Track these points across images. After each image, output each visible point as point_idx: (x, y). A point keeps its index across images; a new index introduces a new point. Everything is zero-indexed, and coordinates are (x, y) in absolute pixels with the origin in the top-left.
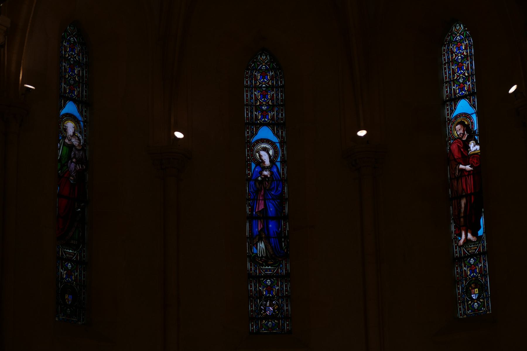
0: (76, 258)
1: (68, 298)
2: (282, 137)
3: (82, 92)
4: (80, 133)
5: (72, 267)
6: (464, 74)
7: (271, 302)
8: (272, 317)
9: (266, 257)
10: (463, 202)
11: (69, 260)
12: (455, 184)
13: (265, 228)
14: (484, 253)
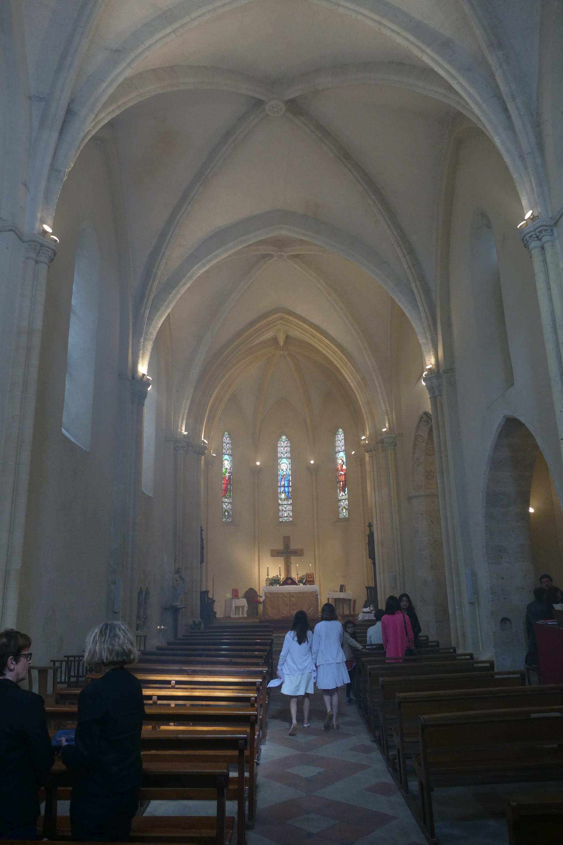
1: (226, 514)
7: (286, 512)
8: (287, 517)
9: (285, 499)
10: (341, 483)
11: (226, 502)
13: (285, 490)
14: (347, 499)
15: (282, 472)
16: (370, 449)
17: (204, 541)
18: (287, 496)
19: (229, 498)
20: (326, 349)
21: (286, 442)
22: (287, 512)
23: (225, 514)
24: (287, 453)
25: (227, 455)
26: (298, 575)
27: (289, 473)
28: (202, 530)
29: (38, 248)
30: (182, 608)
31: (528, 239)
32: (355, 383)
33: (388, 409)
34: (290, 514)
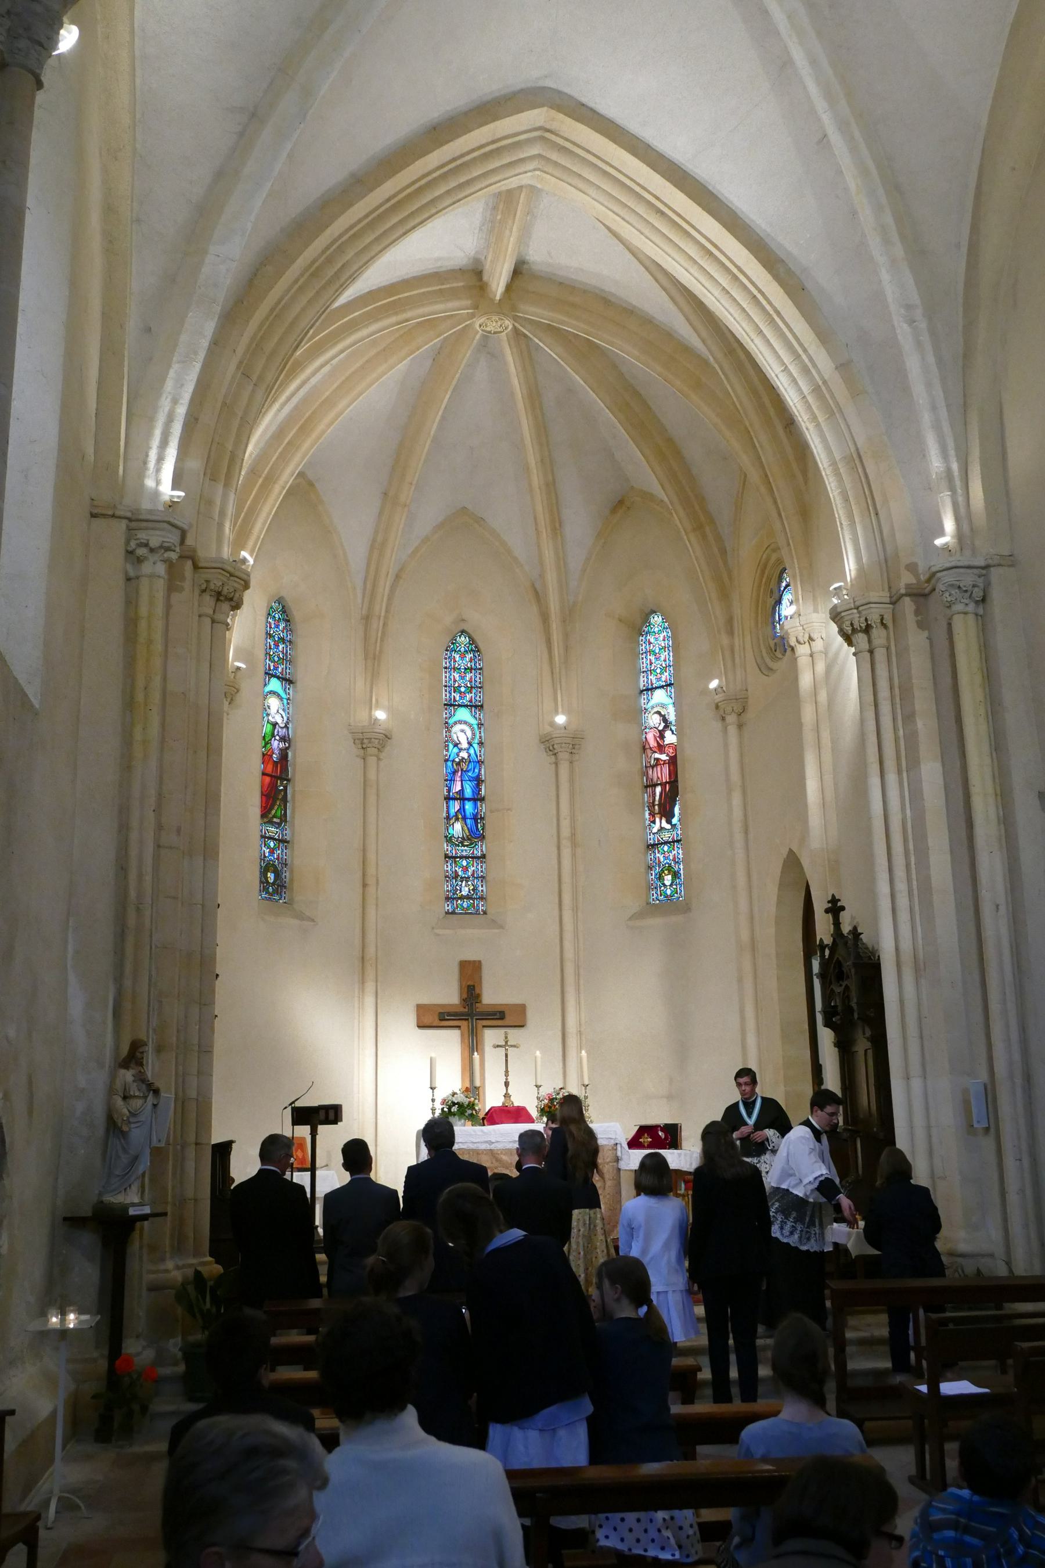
0: (279, 836)
1: (271, 876)
2: (480, 719)
3: (286, 669)
4: (284, 710)
5: (275, 845)
6: (661, 665)
7: (467, 882)
9: (463, 838)
10: (658, 789)
12: (650, 772)
13: (462, 809)
15: (456, 750)
16: (866, 620)
18: (470, 830)
19: (279, 824)
20: (701, 263)
21: (469, 656)
22: (469, 883)
24: (474, 691)
25: (278, 678)
26: (538, 1087)
27: (478, 754)
30: (144, 1218)
32: (806, 389)
33: (955, 466)
34: (480, 888)
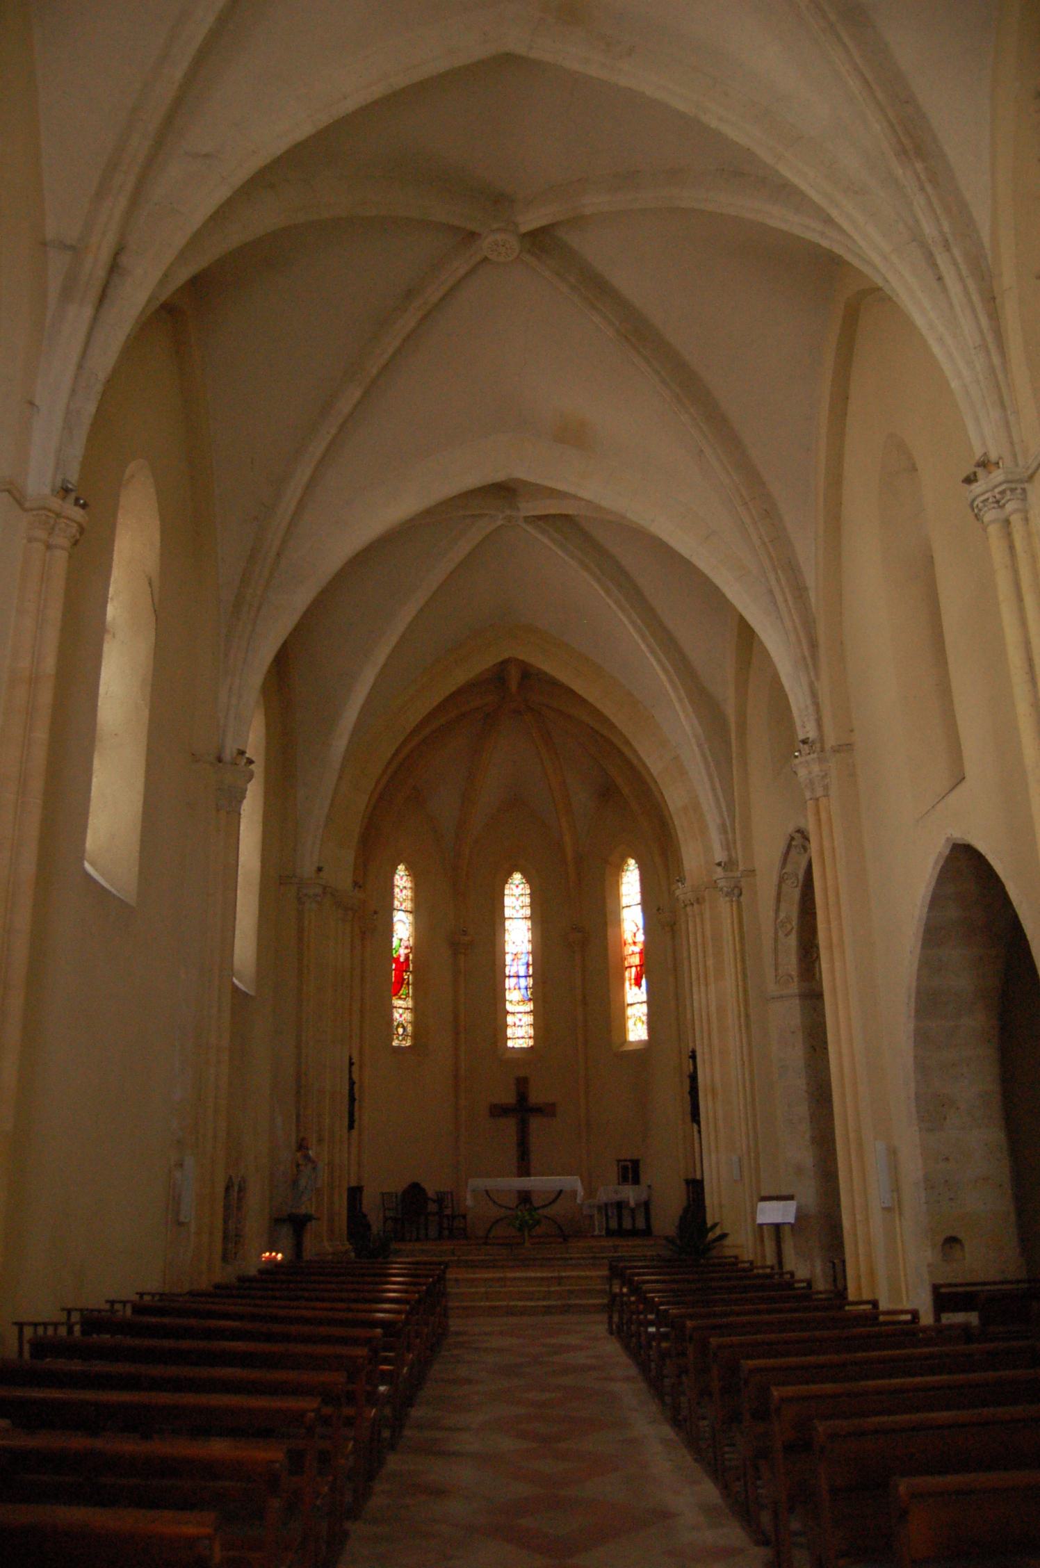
1: (400, 1030)
13: (518, 983)
17: (356, 1087)
19: (405, 999)
23: (397, 1031)
28: (351, 1064)
29: (52, 521)
31: (981, 505)
